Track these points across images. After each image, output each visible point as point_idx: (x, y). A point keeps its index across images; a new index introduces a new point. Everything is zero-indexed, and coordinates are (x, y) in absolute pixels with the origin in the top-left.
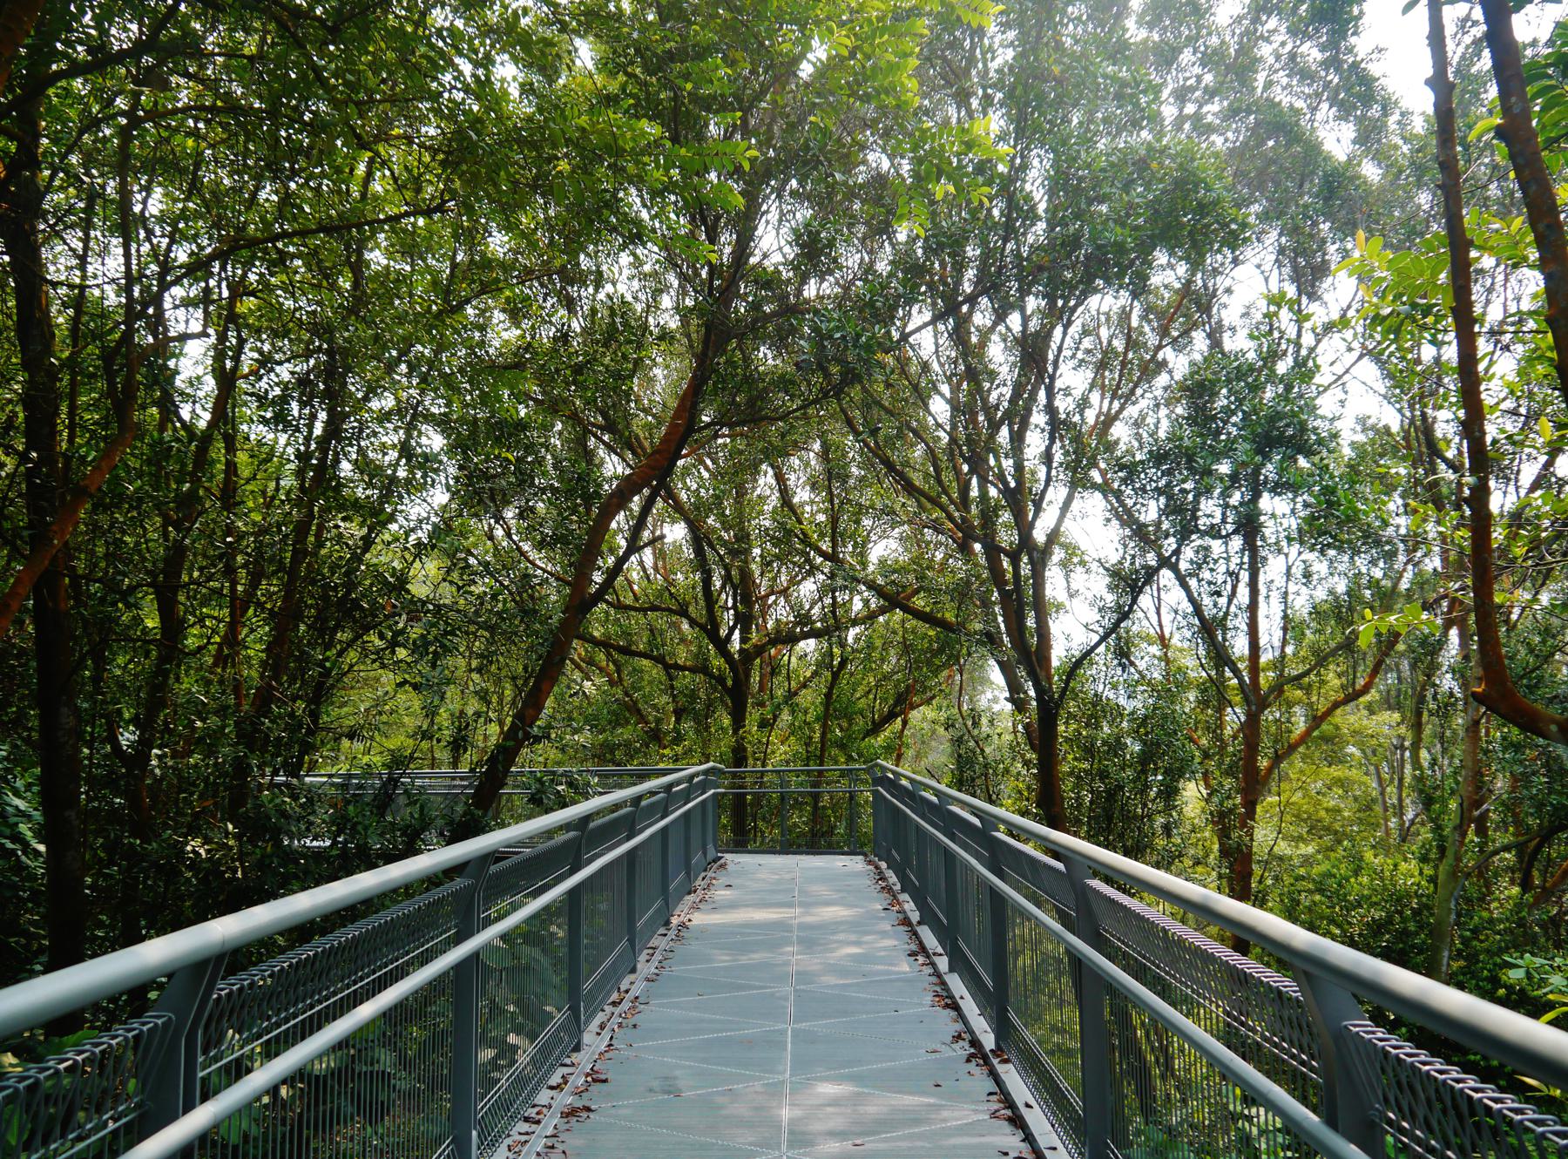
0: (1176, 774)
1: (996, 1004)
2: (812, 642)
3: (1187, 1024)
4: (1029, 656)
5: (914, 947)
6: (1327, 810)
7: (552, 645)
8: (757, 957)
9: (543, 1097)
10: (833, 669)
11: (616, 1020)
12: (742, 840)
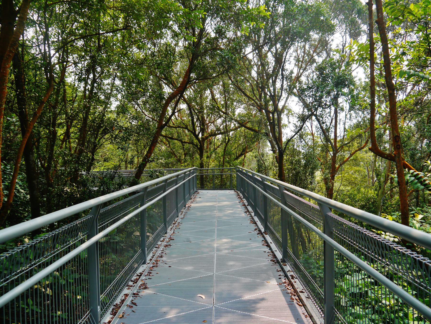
0: (314, 168)
1: (265, 222)
2: (220, 135)
3: (314, 228)
4: (277, 139)
5: (246, 211)
6: (354, 178)
7: (154, 138)
8: (208, 213)
9: (159, 243)
10: (226, 142)
11: (174, 227)
12: (203, 187)
